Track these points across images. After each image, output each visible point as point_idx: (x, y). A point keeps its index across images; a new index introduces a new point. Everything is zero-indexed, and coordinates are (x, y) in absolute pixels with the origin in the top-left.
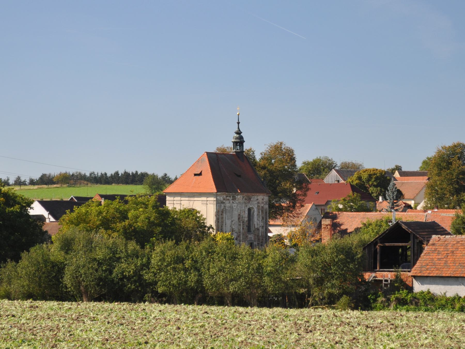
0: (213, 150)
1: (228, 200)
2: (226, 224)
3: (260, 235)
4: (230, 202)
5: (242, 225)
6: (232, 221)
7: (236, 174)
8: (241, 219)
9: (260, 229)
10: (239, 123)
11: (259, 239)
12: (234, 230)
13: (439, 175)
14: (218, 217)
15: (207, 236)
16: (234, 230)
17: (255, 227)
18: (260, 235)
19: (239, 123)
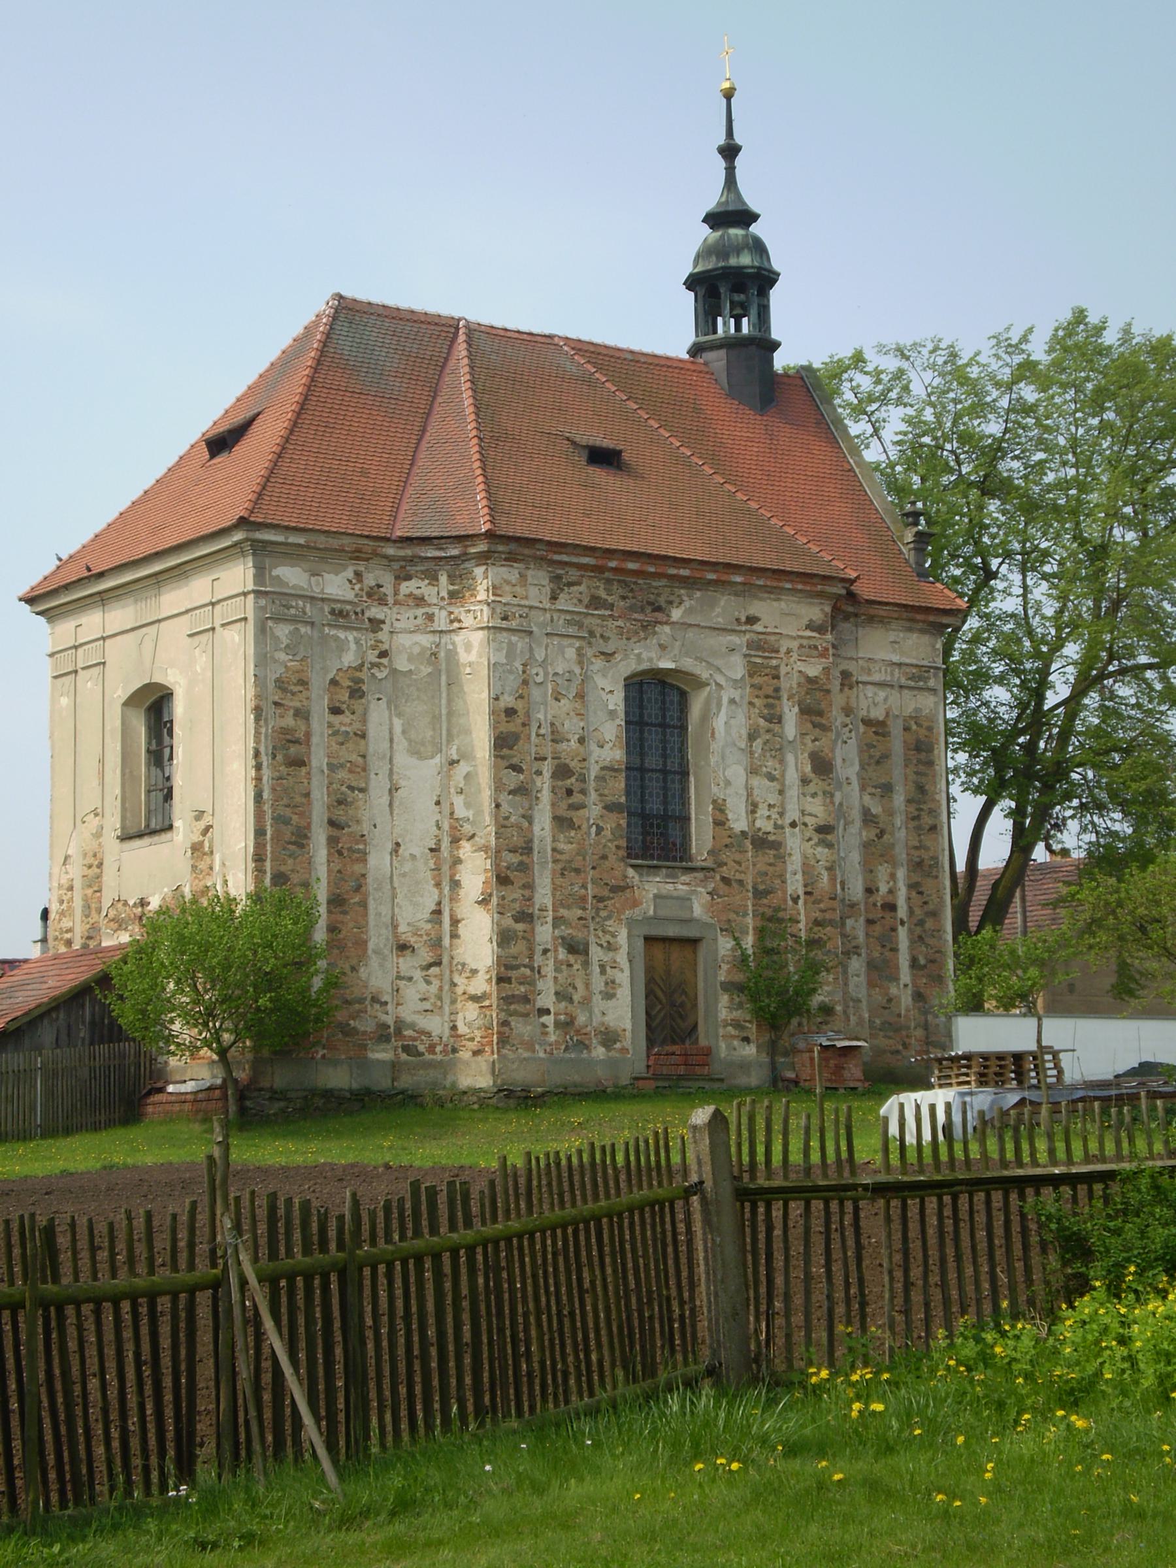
0: (348, 293)
1: (420, 601)
2: (394, 789)
3: (795, 884)
4: (430, 617)
5: (546, 796)
6: (453, 763)
7: (258, 414)
8: (531, 746)
9: (796, 845)
10: (730, 152)
11: (1141, 974)
12: (467, 829)
13: (1049, 352)
14: (673, 764)
15: (532, 921)
16: (467, 829)
17: (719, 823)
18: (795, 884)
19: (730, 152)
